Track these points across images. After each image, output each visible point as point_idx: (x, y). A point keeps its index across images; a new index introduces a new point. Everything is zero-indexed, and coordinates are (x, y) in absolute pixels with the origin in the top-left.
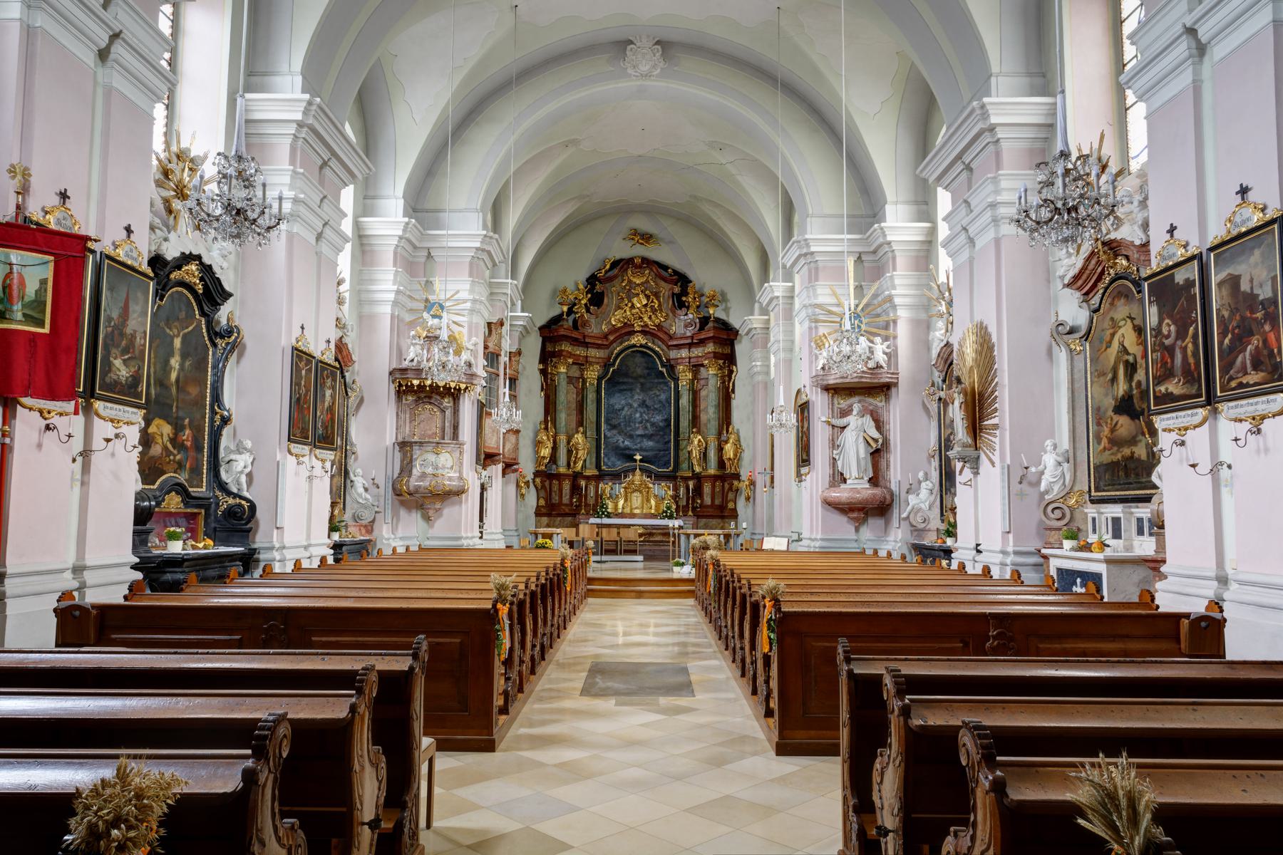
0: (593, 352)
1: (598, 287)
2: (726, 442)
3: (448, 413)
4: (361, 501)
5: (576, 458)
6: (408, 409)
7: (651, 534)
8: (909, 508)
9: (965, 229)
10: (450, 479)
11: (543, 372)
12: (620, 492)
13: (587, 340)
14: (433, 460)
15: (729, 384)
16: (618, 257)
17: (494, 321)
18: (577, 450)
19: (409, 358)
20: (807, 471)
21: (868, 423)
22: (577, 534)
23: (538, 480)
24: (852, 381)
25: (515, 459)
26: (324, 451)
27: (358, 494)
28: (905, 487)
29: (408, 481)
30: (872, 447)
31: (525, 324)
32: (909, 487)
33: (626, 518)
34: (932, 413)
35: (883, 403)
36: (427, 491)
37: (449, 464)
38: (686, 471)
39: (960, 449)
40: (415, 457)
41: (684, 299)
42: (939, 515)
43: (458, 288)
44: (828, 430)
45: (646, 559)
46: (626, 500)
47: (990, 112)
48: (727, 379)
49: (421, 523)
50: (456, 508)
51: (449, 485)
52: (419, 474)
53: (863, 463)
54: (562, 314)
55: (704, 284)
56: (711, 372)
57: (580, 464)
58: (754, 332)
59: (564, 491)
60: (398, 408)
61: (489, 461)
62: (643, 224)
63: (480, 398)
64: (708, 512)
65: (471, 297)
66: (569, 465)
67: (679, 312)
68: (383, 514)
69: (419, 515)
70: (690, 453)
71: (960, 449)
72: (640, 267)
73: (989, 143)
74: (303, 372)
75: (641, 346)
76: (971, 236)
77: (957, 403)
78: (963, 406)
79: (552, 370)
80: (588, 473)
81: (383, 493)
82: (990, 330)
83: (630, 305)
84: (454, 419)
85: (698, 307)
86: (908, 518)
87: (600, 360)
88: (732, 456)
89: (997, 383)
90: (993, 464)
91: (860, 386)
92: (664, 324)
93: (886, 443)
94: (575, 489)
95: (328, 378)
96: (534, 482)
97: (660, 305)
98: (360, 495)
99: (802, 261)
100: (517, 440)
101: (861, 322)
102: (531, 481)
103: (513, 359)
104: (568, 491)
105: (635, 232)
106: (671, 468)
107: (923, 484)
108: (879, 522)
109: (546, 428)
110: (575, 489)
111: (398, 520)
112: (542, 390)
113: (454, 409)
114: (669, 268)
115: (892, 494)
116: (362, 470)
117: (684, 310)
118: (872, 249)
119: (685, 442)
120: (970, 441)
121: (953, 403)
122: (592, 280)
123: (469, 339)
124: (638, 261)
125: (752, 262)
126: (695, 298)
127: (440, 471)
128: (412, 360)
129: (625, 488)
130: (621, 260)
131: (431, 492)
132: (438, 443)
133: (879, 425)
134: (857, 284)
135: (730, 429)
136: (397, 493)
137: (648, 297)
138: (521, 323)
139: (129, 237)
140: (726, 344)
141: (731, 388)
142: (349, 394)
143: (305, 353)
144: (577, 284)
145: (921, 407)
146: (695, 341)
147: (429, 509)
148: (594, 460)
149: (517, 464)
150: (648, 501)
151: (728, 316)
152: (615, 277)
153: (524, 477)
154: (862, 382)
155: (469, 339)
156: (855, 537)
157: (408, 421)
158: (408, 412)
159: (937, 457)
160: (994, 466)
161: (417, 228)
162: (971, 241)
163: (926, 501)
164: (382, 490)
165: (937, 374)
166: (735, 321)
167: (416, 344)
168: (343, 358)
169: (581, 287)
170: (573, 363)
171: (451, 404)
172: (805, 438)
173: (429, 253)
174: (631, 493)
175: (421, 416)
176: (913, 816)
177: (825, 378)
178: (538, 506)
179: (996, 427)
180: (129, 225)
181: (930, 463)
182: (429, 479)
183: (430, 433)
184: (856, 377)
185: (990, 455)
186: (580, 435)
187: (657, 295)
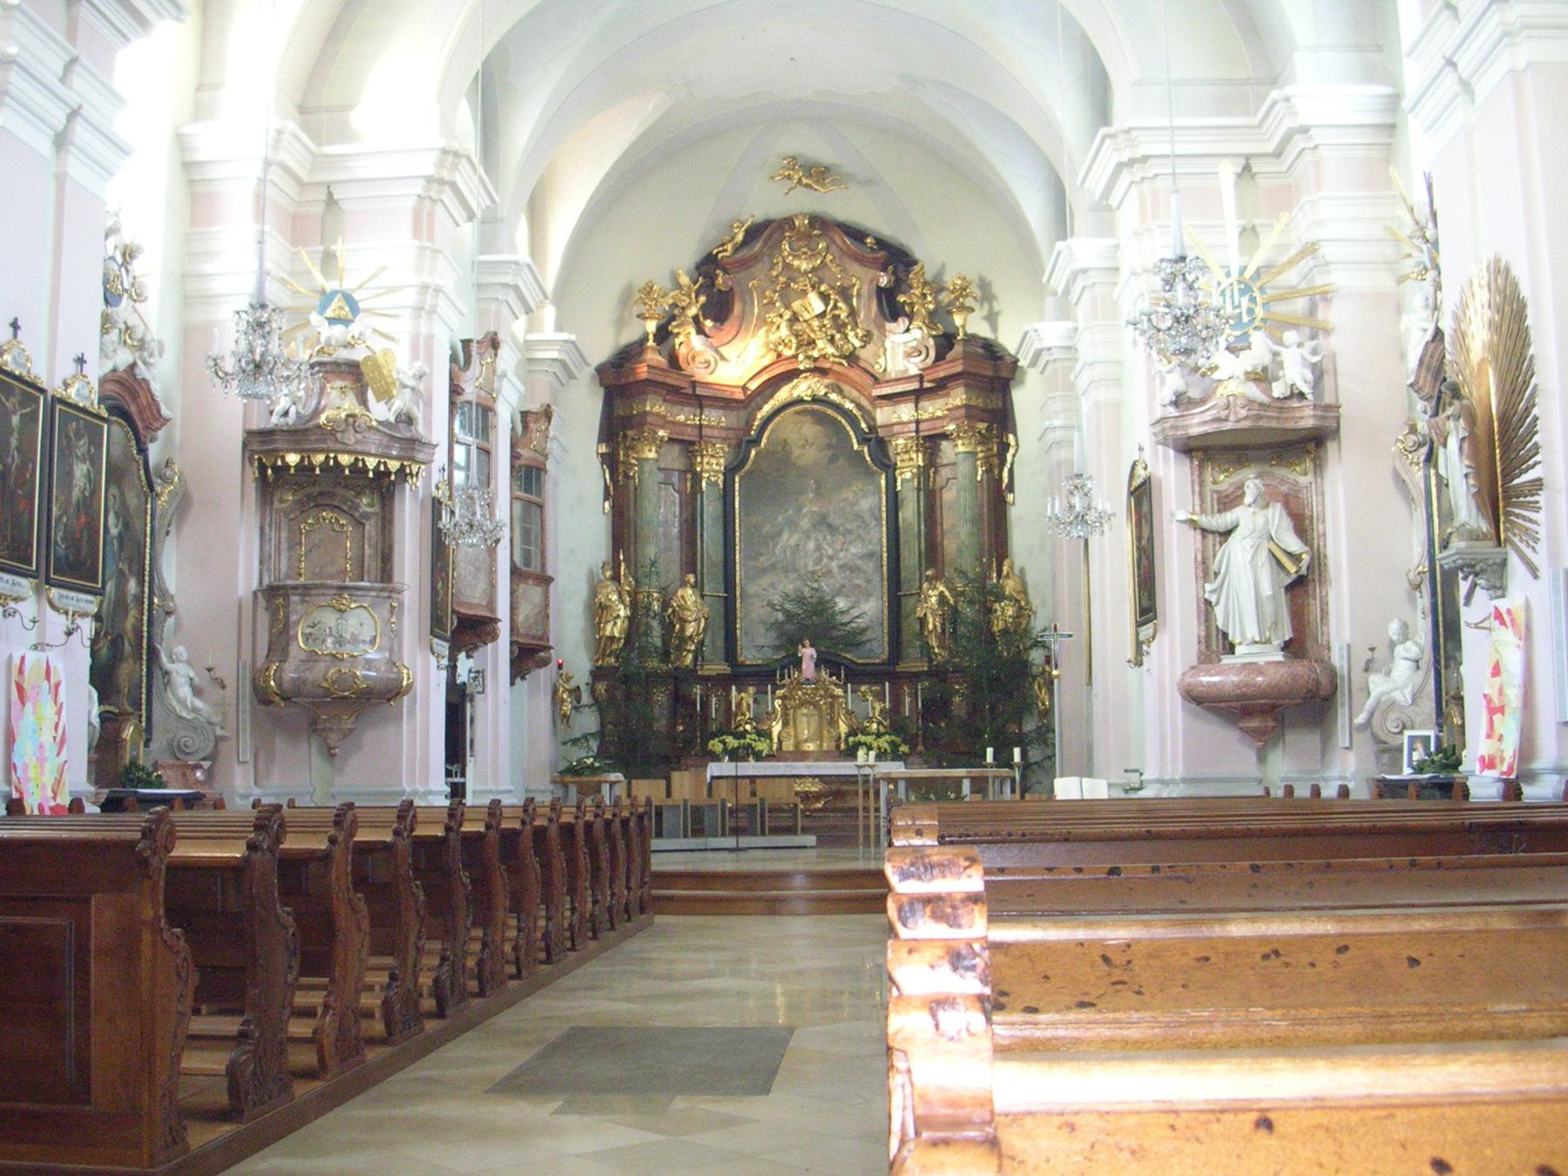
0: (712, 417)
1: (720, 280)
3: (371, 527)
4: (184, 714)
7: (839, 794)
8: (1370, 702)
9: (1451, 63)
10: (369, 664)
11: (610, 461)
12: (774, 708)
13: (699, 391)
14: (333, 624)
16: (760, 216)
18: (683, 621)
19: (279, 409)
20: (1151, 632)
21: (1276, 517)
22: (669, 794)
23: (601, 687)
24: (1239, 426)
25: (541, 639)
26: (73, 594)
28: (1362, 656)
30: (1288, 573)
31: (563, 356)
32: (1369, 655)
34: (1413, 492)
35: (1310, 478)
36: (319, 691)
37: (367, 634)
38: (915, 660)
39: (1463, 544)
40: (294, 618)
41: (902, 298)
42: (1434, 716)
44: (1194, 538)
45: (821, 843)
46: (785, 724)
48: (996, 461)
49: (317, 760)
51: (366, 677)
52: (303, 656)
53: (1269, 609)
54: (645, 338)
55: (943, 266)
56: (961, 449)
58: (1044, 358)
60: (263, 518)
62: (818, 150)
67: (889, 326)
68: (233, 742)
69: (314, 749)
70: (923, 621)
71: (1463, 544)
74: (15, 420)
76: (1464, 76)
77: (1453, 443)
78: (1466, 446)
79: (627, 456)
82: (1515, 272)
83: (787, 315)
84: (384, 539)
85: (931, 314)
86: (1368, 724)
89: (1536, 386)
90: (1534, 571)
91: (1260, 440)
93: (1318, 563)
94: (680, 701)
95: (79, 436)
96: (593, 692)
97: (853, 313)
98: (183, 703)
99: (1125, 178)
100: (546, 598)
101: (1253, 300)
103: (532, 426)
105: (794, 162)
107: (1400, 650)
108: (1312, 739)
110: (680, 701)
111: (271, 757)
112: (607, 497)
113: (384, 518)
114: (868, 235)
115: (1333, 674)
116: (187, 648)
117: (903, 323)
118: (1270, 147)
119: (912, 601)
120: (1485, 526)
121: (1445, 446)
122: (708, 266)
125: (1034, 208)
126: (924, 296)
127: (348, 650)
128: (286, 414)
129: (783, 698)
131: (328, 693)
132: (342, 588)
133: (1302, 524)
134: (1243, 222)
135: (1005, 569)
136: (262, 697)
137: (825, 297)
138: (555, 355)
139: (15, 336)
140: (993, 390)
142: (158, 489)
143: (19, 379)
144: (674, 278)
145: (1390, 481)
146: (927, 385)
148: (720, 643)
150: (833, 723)
151: (994, 329)
152: (756, 258)
153: (568, 679)
154: (1260, 429)
156: (1256, 774)
157: (284, 546)
158: (284, 527)
159: (1426, 588)
160: (1536, 577)
161: (299, 140)
162: (1466, 86)
163: (1405, 687)
164: (230, 692)
165: (1420, 405)
166: (1008, 340)
168: (140, 412)
169: (685, 280)
170: (671, 440)
171: (377, 509)
172: (1145, 562)
173: (330, 194)
174: (795, 708)
177: (1180, 423)
179: (1537, 485)
180: (16, 319)
181: (1412, 602)
182: (322, 665)
183: (332, 570)
184: (1246, 418)
185: (1528, 552)
186: (690, 591)
187: (845, 294)
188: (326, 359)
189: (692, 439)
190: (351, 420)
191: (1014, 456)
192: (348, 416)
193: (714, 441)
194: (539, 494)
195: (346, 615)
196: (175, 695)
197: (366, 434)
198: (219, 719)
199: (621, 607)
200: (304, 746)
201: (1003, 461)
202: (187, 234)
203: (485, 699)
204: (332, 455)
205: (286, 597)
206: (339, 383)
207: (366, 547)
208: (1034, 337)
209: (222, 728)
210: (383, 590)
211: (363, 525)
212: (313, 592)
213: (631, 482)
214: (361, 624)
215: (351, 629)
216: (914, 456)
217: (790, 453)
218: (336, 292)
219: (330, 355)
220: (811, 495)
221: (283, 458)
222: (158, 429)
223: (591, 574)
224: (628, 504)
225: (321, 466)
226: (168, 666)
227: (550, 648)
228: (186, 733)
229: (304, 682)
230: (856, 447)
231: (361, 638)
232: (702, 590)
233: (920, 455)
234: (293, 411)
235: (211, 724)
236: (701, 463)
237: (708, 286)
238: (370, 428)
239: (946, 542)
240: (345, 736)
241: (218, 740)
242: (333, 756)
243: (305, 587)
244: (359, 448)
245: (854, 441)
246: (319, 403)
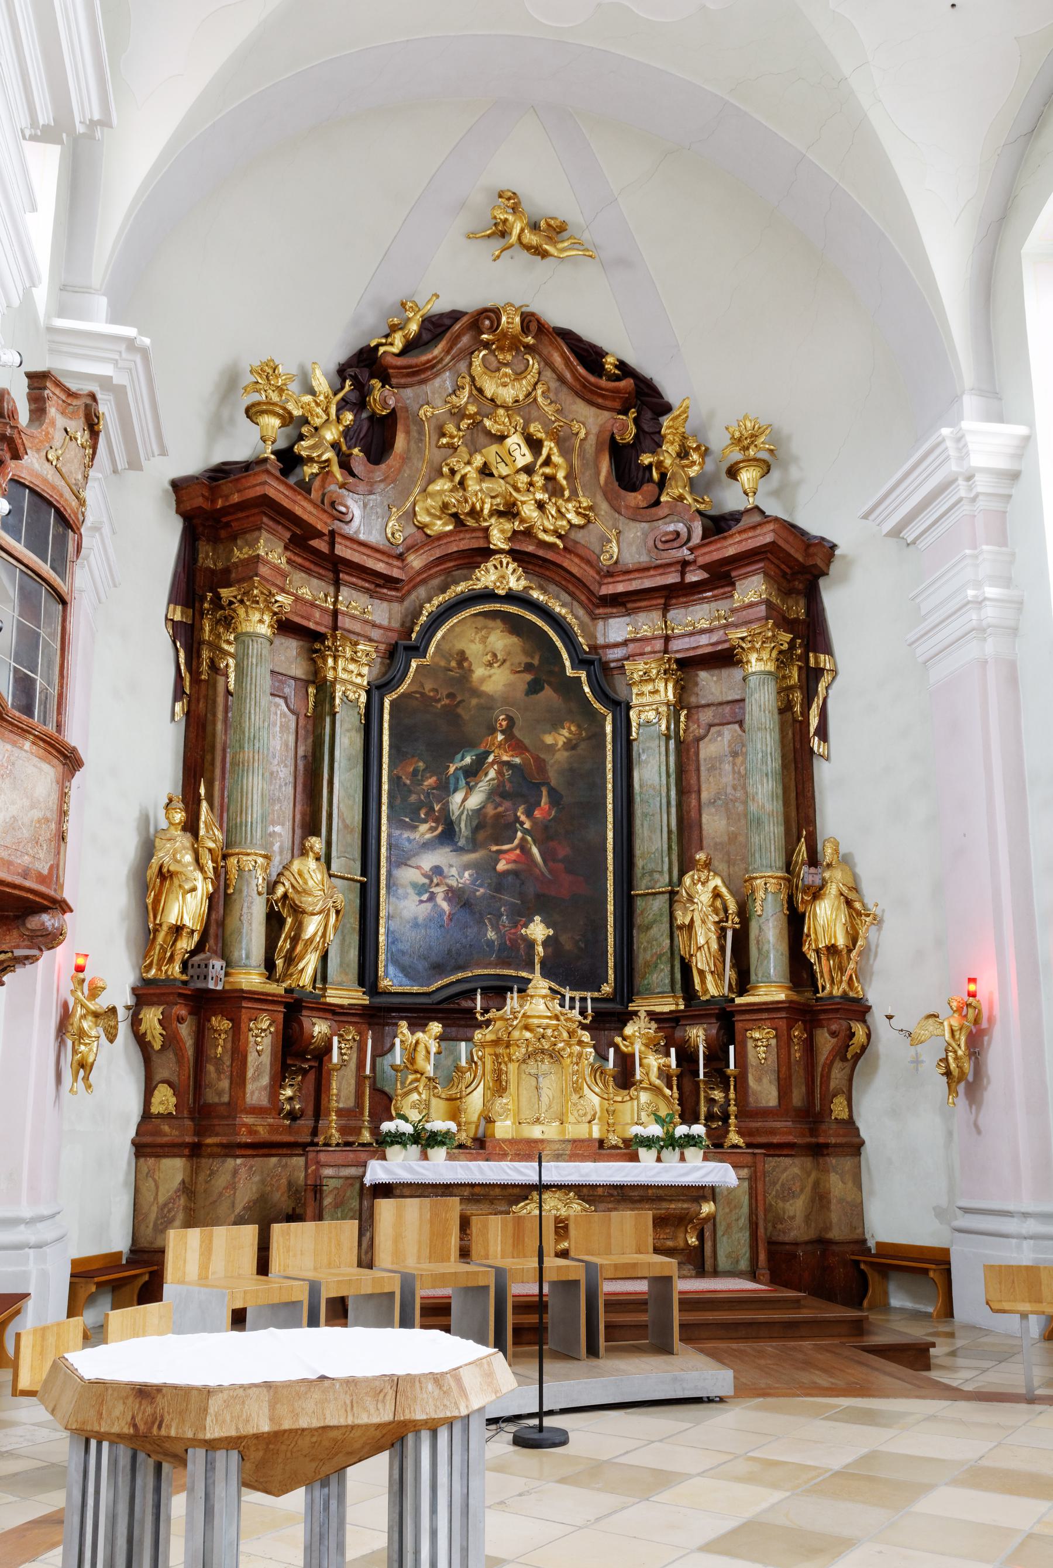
1: (377, 394)
2: (817, 893)
5: (295, 940)
13: (342, 550)
15: (806, 713)
22: (366, 1260)
23: (151, 1017)
25: (42, 879)
33: (503, 1156)
41: (646, 459)
47: (971, 446)
48: (798, 696)
57: (310, 963)
59: (252, 1058)
64: (772, 1132)
66: (269, 965)
72: (515, 345)
73: (960, 500)
75: (511, 597)
80: (335, 997)
87: (375, 634)
88: (841, 941)
92: (578, 536)
96: (135, 1022)
102: (122, 1013)
104: (266, 1059)
106: (607, 989)
109: (191, 827)
112: (176, 699)
124: (510, 322)
130: (455, 316)
137: (534, 444)
141: (814, 722)
153: (95, 992)
169: (322, 383)
178: (147, 1115)
186: (311, 863)
189: (322, 629)
191: (827, 688)
193: (354, 638)
194: (61, 565)
199: (199, 876)
201: (809, 695)
208: (952, 452)
213: (221, 680)
216: (661, 686)
217: (471, 671)
220: (500, 737)
223: (145, 820)
224: (214, 715)
227: (62, 906)
230: (569, 672)
232: (329, 868)
233: (670, 686)
236: (335, 669)
237: (358, 402)
239: (705, 818)
245: (568, 663)
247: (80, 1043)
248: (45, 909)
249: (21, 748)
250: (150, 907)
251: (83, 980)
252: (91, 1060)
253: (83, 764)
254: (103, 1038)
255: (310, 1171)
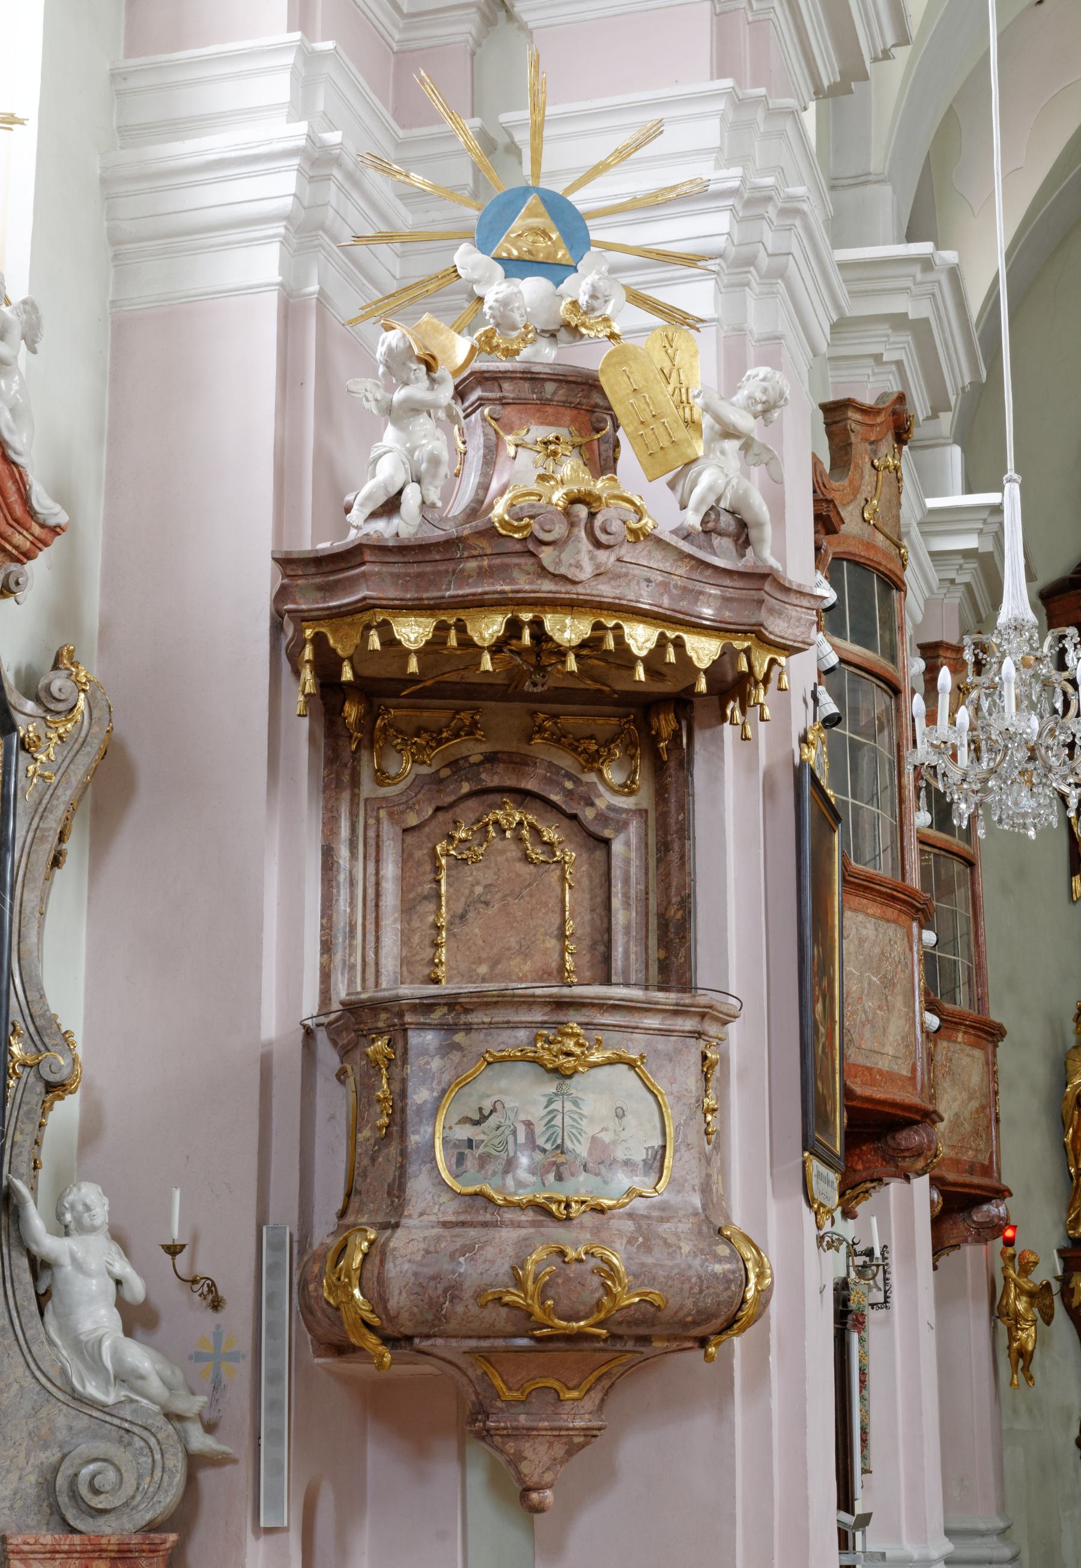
4: (92, 1389)
6: (389, 832)
14: (537, 1113)
17: (867, 399)
25: (986, 1170)
27: (78, 1346)
29: (377, 1253)
40: (420, 1095)
43: (660, 117)
50: (701, 1423)
52: (450, 1210)
61: (869, 1158)
63: (811, 755)
65: (730, 177)
68: (242, 1472)
69: (477, 1477)
81: (245, 1344)
100: (992, 1072)
102: (1056, 1287)
123: (731, 385)
128: (391, 506)
132: (560, 1004)
138: (970, 542)
147: (527, 1433)
149: (1002, 1193)
153: (1026, 1269)
155: (731, 385)
167: (414, 408)
171: (644, 798)
175: (470, 874)
176: (177, 1194)
188: (500, 364)
190: (582, 511)
192: (575, 500)
195: (574, 1085)
196: (68, 1330)
197: (626, 552)
198: (200, 1401)
200: (446, 1471)
202: (116, 76)
203: (888, 1322)
204: (526, 616)
205: (398, 1034)
206: (539, 432)
207: (616, 902)
209: (210, 1428)
210: (678, 1012)
211: (607, 843)
212: (474, 1018)
214: (620, 1114)
215: (590, 1129)
218: (526, 191)
219: (510, 353)
221: (385, 628)
222: (29, 556)
225: (496, 649)
226: (48, 1244)
227: (1002, 1193)
228: (102, 1448)
229: (453, 1291)
231: (620, 1154)
234: (411, 498)
235: (173, 1417)
238: (637, 535)
240: (572, 1450)
241: (195, 1462)
242: (537, 1509)
243: (452, 1003)
244: (606, 591)
246: (484, 487)
247: (1018, 1329)
248: (987, 1200)
249: (955, 1042)
250: (1069, 1147)
251: (1014, 1256)
252: (1030, 1347)
253: (1005, 1032)
254: (1040, 1321)
255: (360, 1137)
